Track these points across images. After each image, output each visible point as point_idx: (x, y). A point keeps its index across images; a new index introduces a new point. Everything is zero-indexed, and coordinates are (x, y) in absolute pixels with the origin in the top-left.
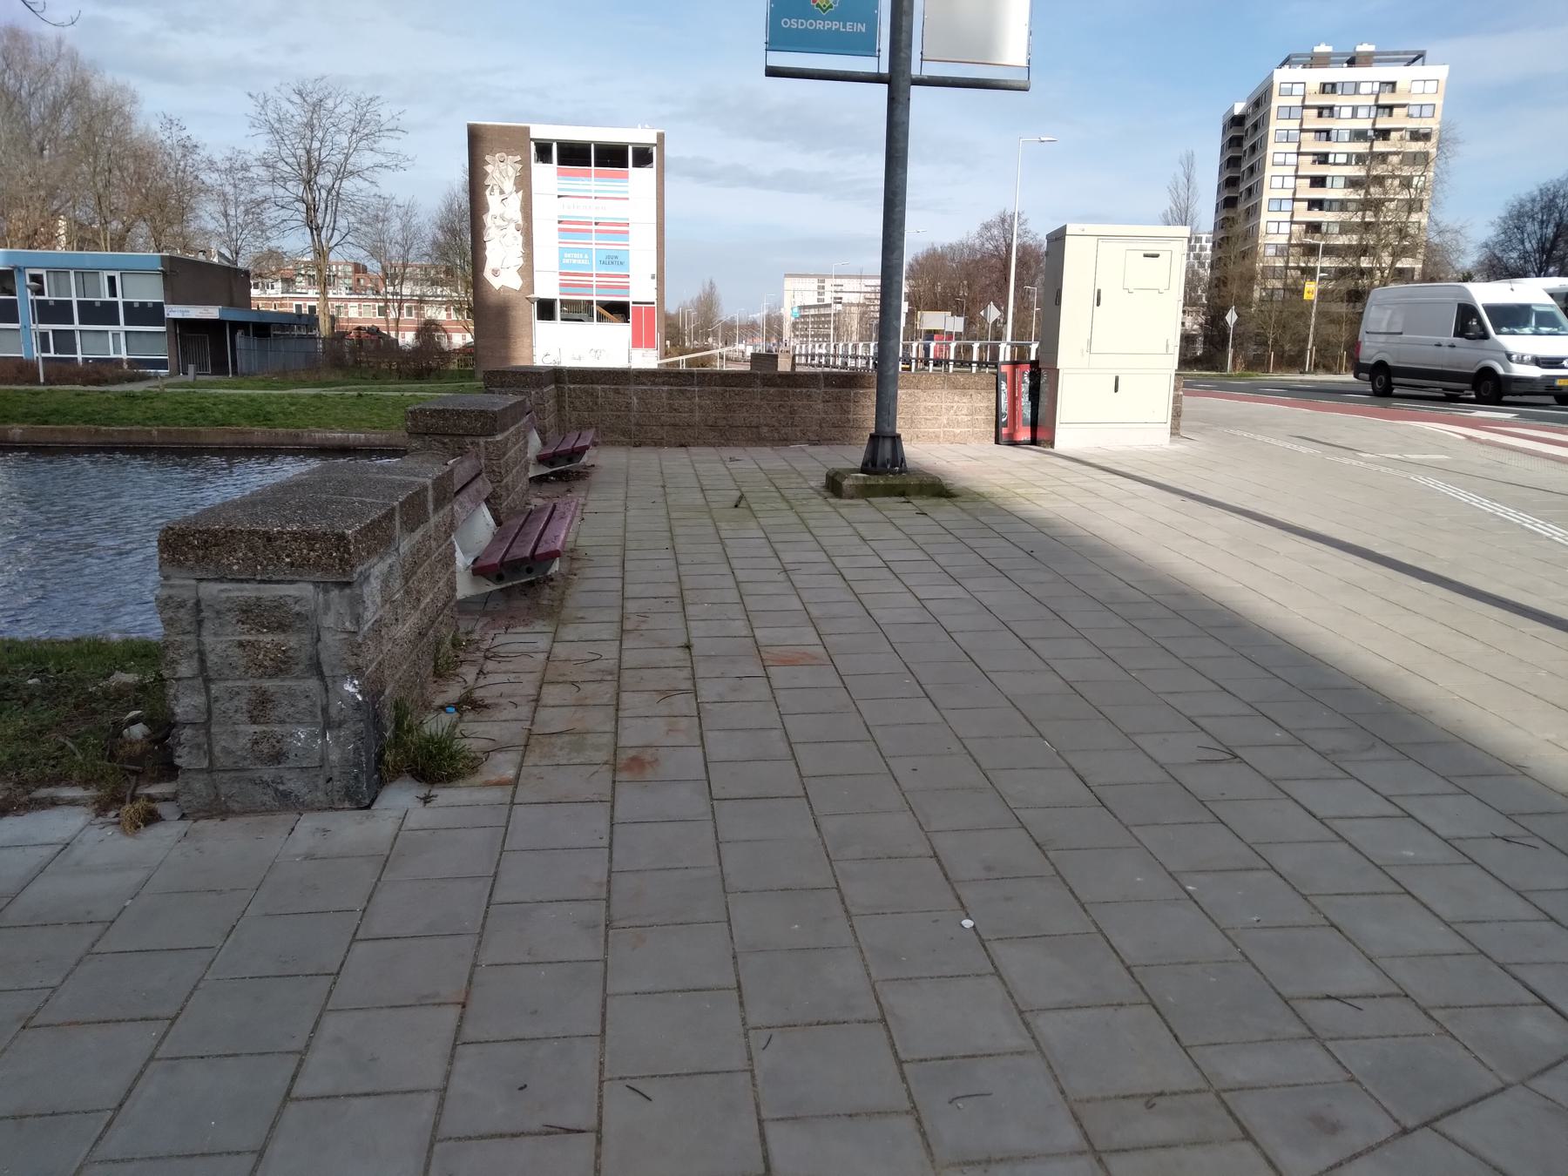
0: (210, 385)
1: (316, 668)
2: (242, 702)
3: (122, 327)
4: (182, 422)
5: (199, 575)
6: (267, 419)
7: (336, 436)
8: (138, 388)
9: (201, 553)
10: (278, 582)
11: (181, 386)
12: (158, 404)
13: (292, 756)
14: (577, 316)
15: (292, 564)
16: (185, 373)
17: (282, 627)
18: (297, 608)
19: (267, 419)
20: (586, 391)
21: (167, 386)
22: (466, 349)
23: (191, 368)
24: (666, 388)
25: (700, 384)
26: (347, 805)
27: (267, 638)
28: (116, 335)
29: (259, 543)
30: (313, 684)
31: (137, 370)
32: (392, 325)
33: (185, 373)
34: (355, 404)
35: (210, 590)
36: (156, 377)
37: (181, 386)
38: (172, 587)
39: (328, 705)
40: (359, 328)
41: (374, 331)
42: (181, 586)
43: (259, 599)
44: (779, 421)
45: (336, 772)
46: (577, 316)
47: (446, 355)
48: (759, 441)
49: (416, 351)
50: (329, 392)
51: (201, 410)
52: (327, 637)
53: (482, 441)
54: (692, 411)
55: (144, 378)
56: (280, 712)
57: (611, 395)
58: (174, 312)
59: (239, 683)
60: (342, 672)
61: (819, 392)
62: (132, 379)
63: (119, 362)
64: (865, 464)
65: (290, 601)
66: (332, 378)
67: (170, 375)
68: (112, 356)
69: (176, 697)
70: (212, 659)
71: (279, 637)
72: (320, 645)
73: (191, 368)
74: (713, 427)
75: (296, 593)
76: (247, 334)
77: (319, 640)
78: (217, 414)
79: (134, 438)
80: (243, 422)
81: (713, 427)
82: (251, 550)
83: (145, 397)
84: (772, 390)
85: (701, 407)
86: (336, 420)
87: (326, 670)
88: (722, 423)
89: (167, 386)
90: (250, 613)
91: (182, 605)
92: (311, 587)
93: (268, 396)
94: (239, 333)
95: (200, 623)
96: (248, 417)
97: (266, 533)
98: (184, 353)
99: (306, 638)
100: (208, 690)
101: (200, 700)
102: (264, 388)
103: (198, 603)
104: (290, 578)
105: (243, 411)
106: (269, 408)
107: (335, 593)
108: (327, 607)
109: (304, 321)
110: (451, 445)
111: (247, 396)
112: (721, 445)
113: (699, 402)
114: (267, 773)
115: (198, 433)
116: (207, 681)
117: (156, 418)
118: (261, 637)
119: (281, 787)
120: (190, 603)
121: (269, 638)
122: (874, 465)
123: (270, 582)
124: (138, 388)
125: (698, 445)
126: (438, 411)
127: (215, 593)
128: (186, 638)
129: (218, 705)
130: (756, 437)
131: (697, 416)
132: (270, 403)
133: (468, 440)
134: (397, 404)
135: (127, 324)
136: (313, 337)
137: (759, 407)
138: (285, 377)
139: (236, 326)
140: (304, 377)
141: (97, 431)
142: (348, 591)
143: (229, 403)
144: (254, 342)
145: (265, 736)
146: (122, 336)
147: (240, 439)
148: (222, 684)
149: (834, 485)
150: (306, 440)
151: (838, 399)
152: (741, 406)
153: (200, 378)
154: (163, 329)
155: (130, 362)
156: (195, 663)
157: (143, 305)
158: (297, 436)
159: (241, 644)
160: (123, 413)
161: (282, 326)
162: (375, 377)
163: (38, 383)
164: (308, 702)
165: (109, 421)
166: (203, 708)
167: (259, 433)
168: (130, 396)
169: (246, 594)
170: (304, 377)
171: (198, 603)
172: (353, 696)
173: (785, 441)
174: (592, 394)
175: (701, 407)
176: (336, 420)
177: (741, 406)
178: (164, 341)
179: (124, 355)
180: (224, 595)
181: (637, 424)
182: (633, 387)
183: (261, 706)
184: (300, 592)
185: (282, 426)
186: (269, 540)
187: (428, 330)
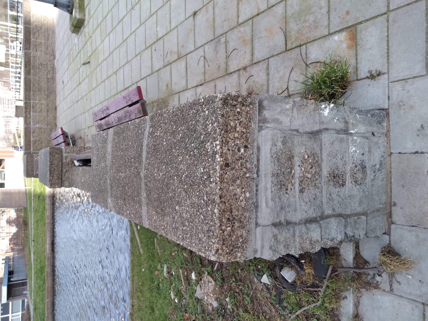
0: (31, 286)
1: (314, 135)
2: (335, 190)
3: (10, 315)
4: (44, 293)
5: (253, 226)
6: (42, 268)
7: (48, 247)
8: (32, 308)
9: (237, 224)
10: (258, 160)
11: (31, 295)
12: (38, 300)
13: (363, 158)
14: (3, 176)
15: (246, 147)
16: (27, 294)
17: (291, 158)
18: (279, 144)
19: (42, 268)
20: (34, 144)
21: (31, 299)
22: (17, 211)
23: (25, 292)
24: (32, 113)
25: (30, 100)
26: (385, 124)
27: (297, 171)
28: (13, 316)
29: (229, 174)
30: (326, 137)
31: (26, 309)
32: (8, 235)
33: (27, 294)
34: (37, 242)
35: (265, 215)
36: (28, 302)
37: (31, 295)
38: (263, 247)
39: (335, 130)
40: (10, 244)
41: (11, 240)
42: (263, 240)
43: (273, 175)
44: (45, 70)
45: (370, 129)
46: (3, 176)
47: (18, 217)
48: (53, 79)
49: (17, 226)
50: (32, 251)
51: (40, 288)
52: (297, 124)
53: (65, 155)
54: (41, 104)
55: (28, 306)
56: (340, 164)
57: (35, 135)
58: (4, 300)
59: (324, 193)
60: (317, 116)
61: (32, 53)
62: (28, 309)
63: (23, 315)
64: (68, 11)
65: (274, 149)
66: (28, 250)
67: (27, 298)
68: (20, 316)
69: (332, 240)
70: (312, 214)
71: (297, 161)
72: (301, 131)
73: (25, 292)
74: (48, 96)
75: (269, 144)
76: (12, 277)
77: (297, 131)
78: (41, 283)
79: (49, 306)
80: (43, 275)
81: (48, 96)
82: (235, 181)
83: (35, 304)
84: (32, 71)
85: (40, 100)
86: (42, 247)
87: (316, 128)
88: (46, 93)
89: (31, 299)
90: (282, 183)
91: (275, 237)
92: (263, 132)
93: (34, 268)
94: (12, 280)
95: (288, 223)
96: (42, 273)
97: (221, 169)
98: (19, 295)
99: (297, 140)
100: (328, 217)
101: (333, 222)
102: (31, 270)
103: (275, 225)
104: (255, 150)
105: (40, 275)
106: (39, 267)
107: (266, 114)
108: (277, 121)
109: (7, 261)
110: (67, 169)
111: (34, 274)
112: (55, 94)
113: (39, 101)
114: (370, 175)
115: (48, 288)
116: (323, 217)
117: (43, 300)
118: (297, 175)
119: (378, 166)
120: (275, 231)
121: (297, 168)
122: (69, 6)
123: (258, 166)
124: (32, 308)
125: (56, 103)
126: (51, 173)
127: (268, 211)
128: (297, 233)
129: (336, 209)
130: (52, 80)
131: (44, 102)
132: (37, 267)
133: (64, 161)
134: (36, 229)
135: (8, 313)
136: (13, 258)
137: (39, 78)
138: (27, 264)
139: (9, 281)
140: (27, 259)
141: (47, 317)
142: (265, 103)
143: (37, 279)
144: (15, 275)
145: (353, 176)
146: (13, 314)
147: (49, 275)
148: (325, 206)
149: (77, 26)
150: (50, 255)
151: (35, 46)
152: (39, 85)
153: (28, 289)
154: (11, 303)
155: (22, 311)
156: (313, 226)
157: (2, 310)
158: (48, 258)
159: (301, 191)
160: (41, 310)
161: (9, 267)
162: (27, 237)
163: (12, 313)
164: (336, 143)
165: (44, 314)
166: (338, 220)
167: (48, 269)
168: (35, 309)
169: (269, 185)
170: (27, 259)
171: (275, 225)
172: (332, 110)
173: (53, 69)
174: (35, 142)
175: (40, 100)
176: (42, 247)
177: (39, 85)
178: (15, 302)
179: (20, 313)
180: (271, 203)
181: (47, 125)
182: (32, 126)
183: (337, 178)
184: (266, 142)
185: (45, 263)
186: (227, 165)
187: (9, 222)
